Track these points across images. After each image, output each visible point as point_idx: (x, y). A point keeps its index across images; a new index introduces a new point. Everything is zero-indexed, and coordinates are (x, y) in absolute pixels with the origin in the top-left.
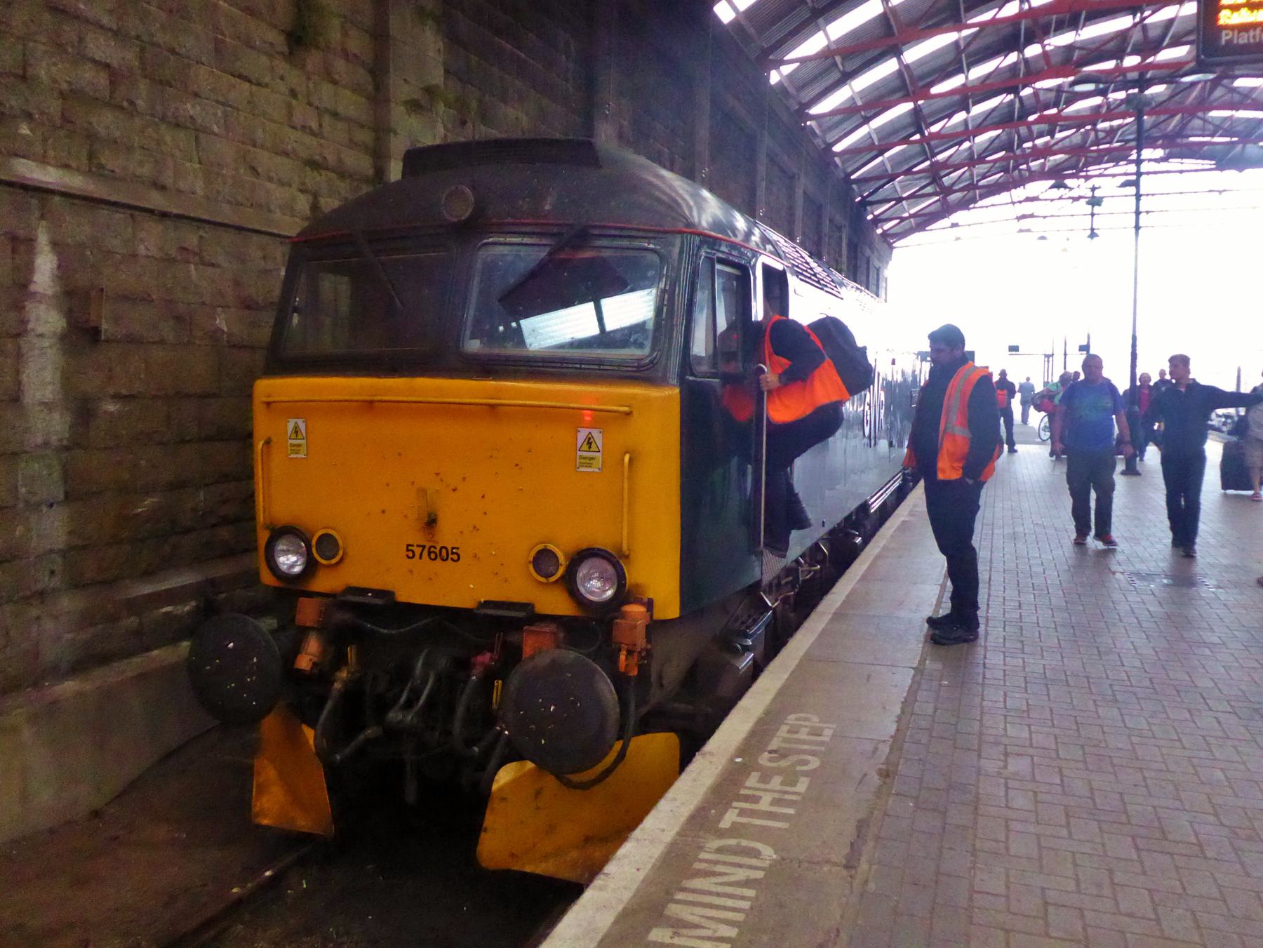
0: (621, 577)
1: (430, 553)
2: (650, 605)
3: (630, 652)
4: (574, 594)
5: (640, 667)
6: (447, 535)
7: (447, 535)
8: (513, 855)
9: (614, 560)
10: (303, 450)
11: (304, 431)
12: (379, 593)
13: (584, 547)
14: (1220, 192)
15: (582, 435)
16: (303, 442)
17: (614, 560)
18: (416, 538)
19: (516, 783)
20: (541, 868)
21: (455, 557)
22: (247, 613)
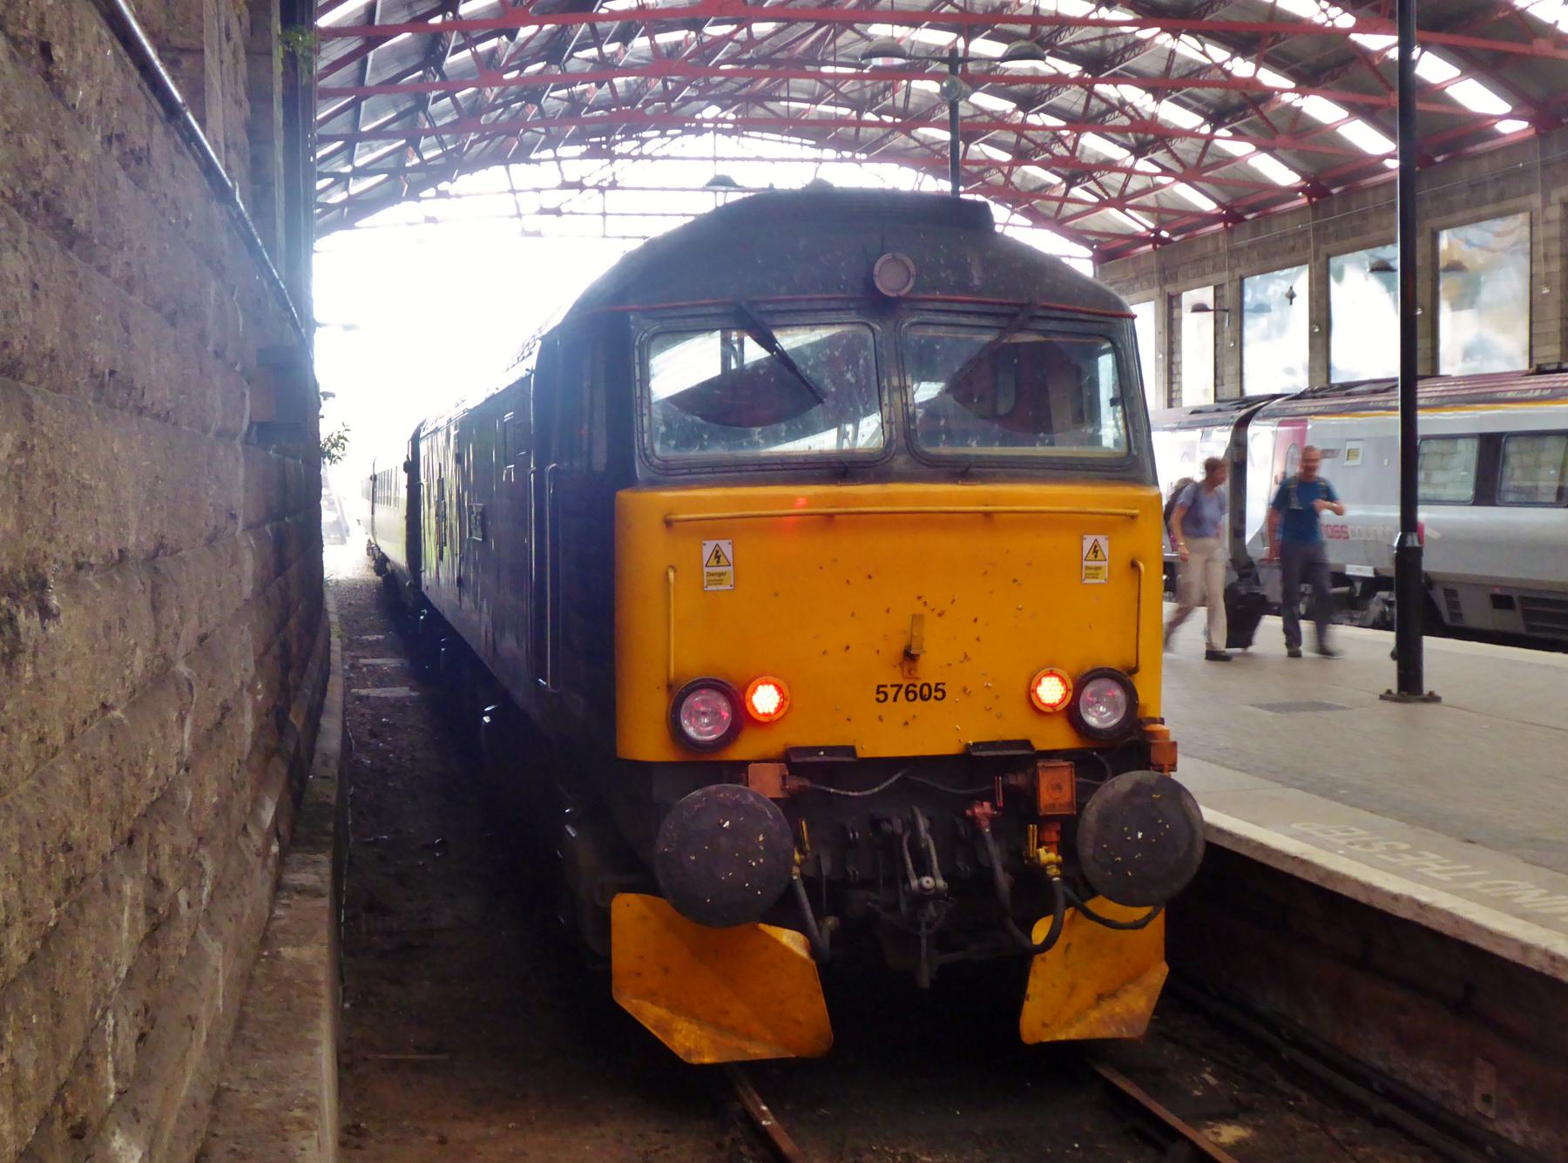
1: (907, 693)
6: (928, 671)
7: (928, 671)
8: (1045, 1025)
10: (729, 579)
11: (1106, 552)
12: (830, 750)
13: (1089, 669)
14: (773, 161)
15: (1088, 543)
16: (1105, 564)
18: (891, 676)
20: (1072, 1033)
21: (939, 694)
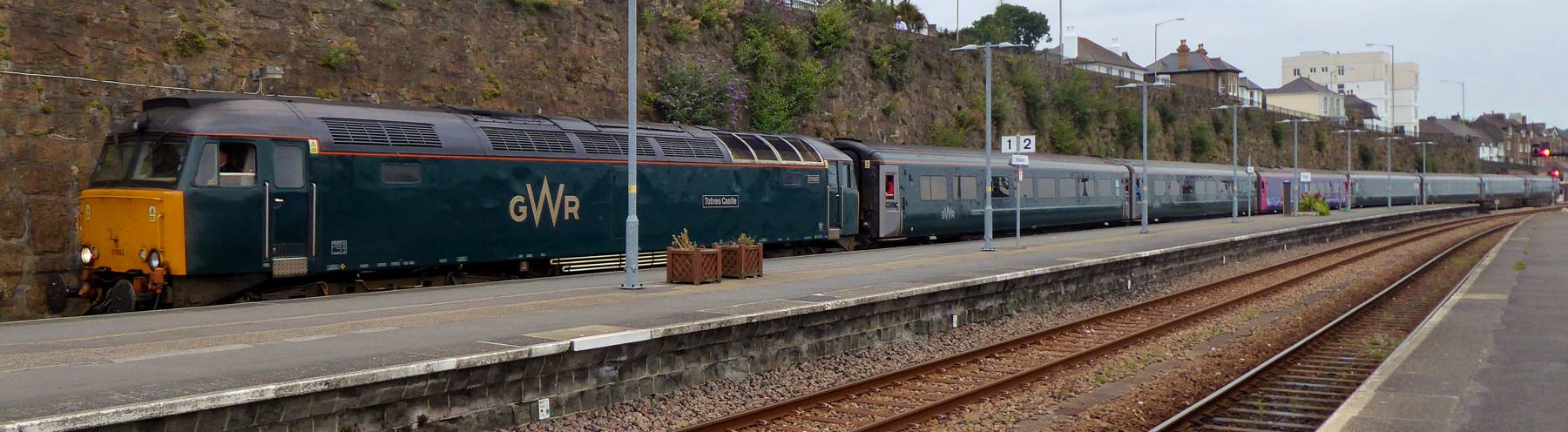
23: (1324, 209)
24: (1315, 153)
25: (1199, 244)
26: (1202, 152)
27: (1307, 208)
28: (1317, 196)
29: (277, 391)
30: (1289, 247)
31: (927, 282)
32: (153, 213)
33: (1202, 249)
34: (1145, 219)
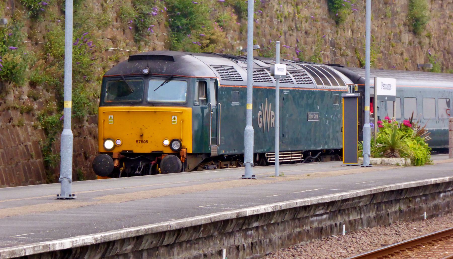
0: (181, 144)
2: (186, 149)
3: (183, 157)
4: (171, 148)
5: (185, 160)
6: (145, 138)
7: (145, 138)
9: (180, 141)
17: (180, 141)
19: (178, 163)
22: (351, 29)
23: (421, 151)
24: (407, 37)
25: (174, 223)
26: (188, 29)
27: (389, 150)
28: (408, 124)
29: (449, 179)
30: (353, 226)
31: (317, 194)
32: (175, 120)
33: (179, 232)
34: (249, 157)
